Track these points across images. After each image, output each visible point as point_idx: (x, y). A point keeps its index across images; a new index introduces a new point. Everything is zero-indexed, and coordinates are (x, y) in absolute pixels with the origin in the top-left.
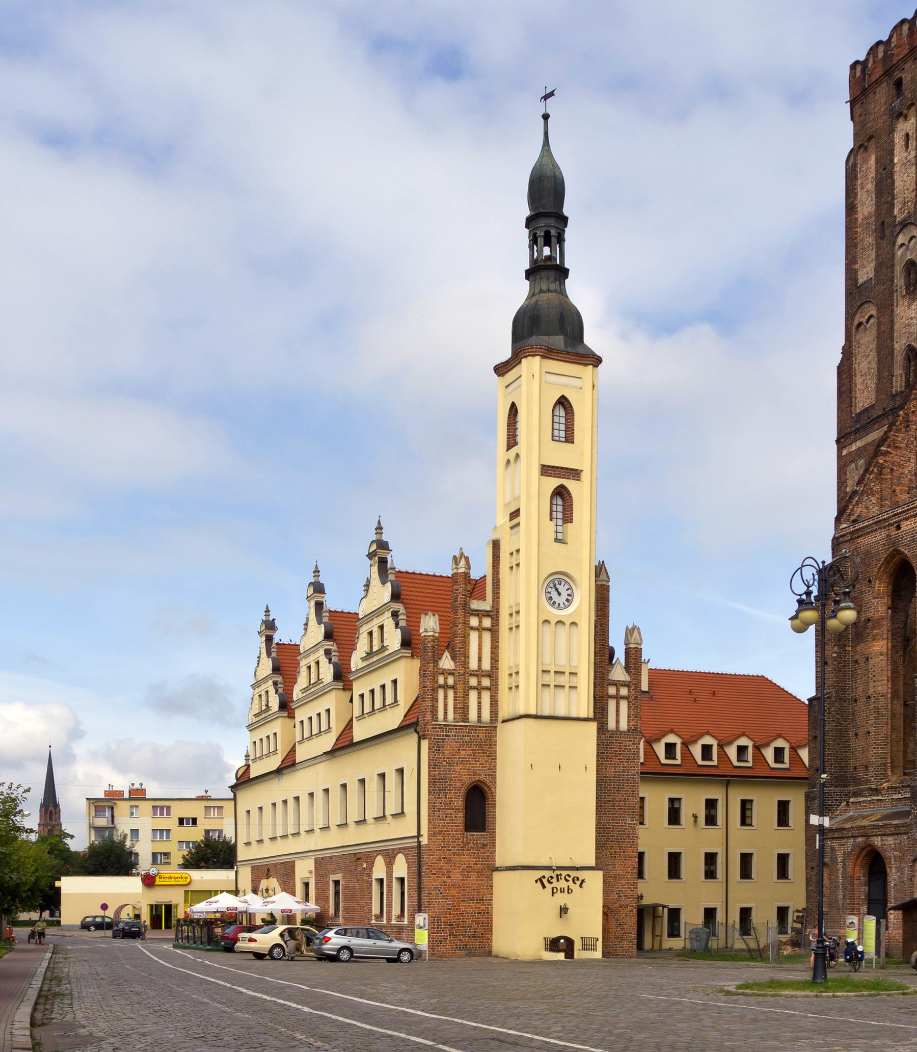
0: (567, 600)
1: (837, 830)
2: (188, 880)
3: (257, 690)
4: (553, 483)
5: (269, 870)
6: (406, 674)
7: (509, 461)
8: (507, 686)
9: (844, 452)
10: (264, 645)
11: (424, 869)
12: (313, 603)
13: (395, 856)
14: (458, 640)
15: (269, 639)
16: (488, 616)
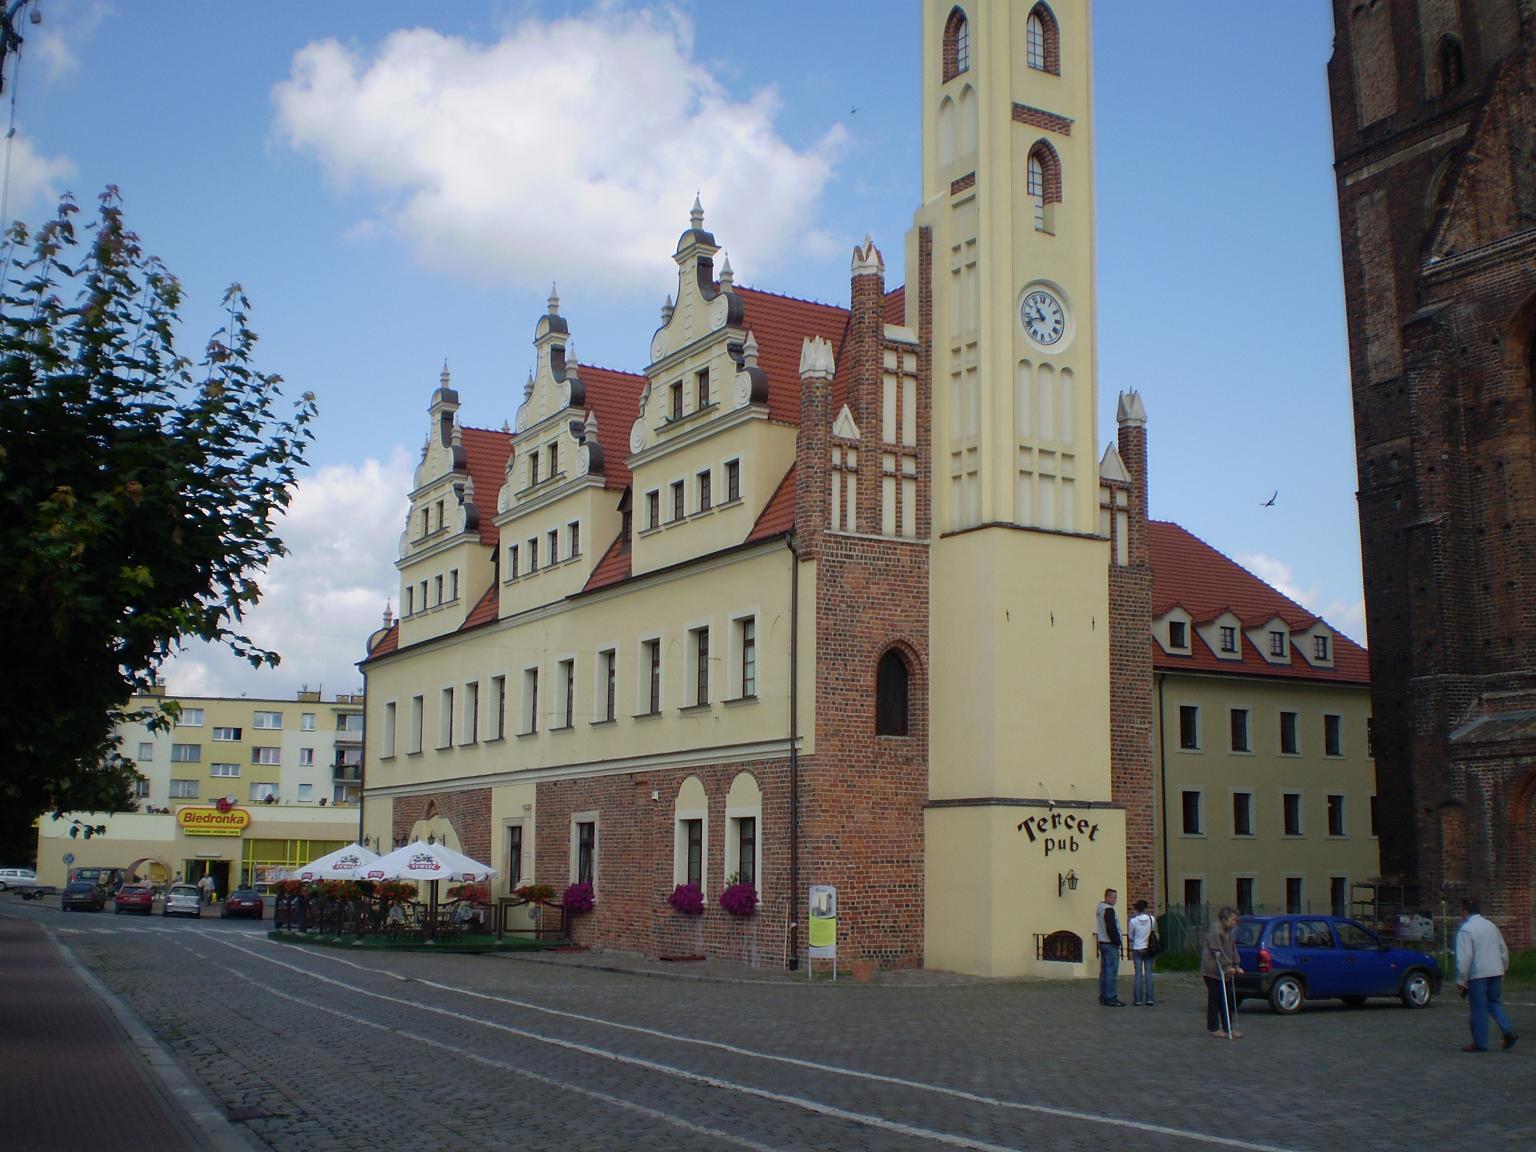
0: (1055, 330)
1: (1480, 745)
2: (245, 822)
3: (420, 502)
4: (1032, 135)
5: (432, 804)
6: (762, 452)
7: (947, 99)
8: (948, 474)
9: (1349, 182)
10: (438, 428)
11: (805, 800)
12: (547, 349)
13: (730, 779)
14: (864, 388)
15: (448, 418)
16: (913, 352)
